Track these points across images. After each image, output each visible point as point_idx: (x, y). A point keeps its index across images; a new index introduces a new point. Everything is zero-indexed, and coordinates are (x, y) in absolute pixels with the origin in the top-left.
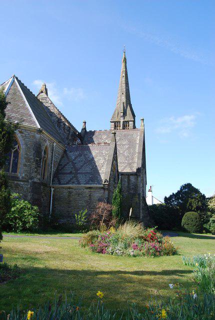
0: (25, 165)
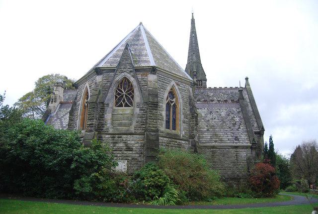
0: (184, 122)
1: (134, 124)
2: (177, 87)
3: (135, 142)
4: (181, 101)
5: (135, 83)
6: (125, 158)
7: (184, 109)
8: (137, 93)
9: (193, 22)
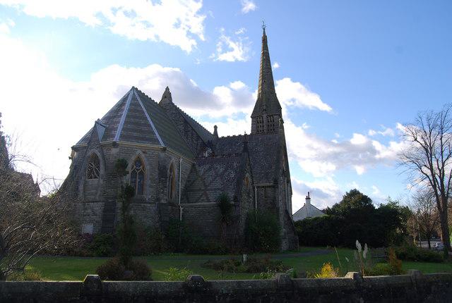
0: (151, 186)
1: (99, 193)
2: (143, 155)
3: (98, 207)
4: (148, 167)
5: (100, 158)
6: (91, 222)
7: (151, 175)
8: (102, 166)
9: (265, 40)
